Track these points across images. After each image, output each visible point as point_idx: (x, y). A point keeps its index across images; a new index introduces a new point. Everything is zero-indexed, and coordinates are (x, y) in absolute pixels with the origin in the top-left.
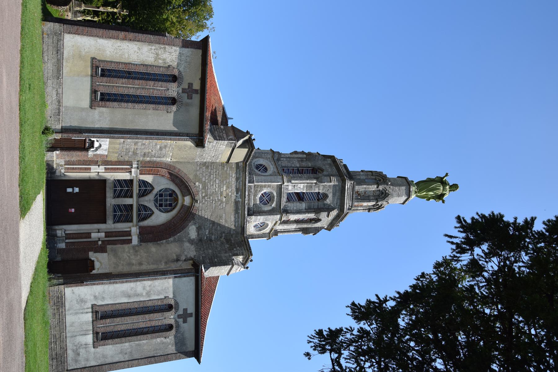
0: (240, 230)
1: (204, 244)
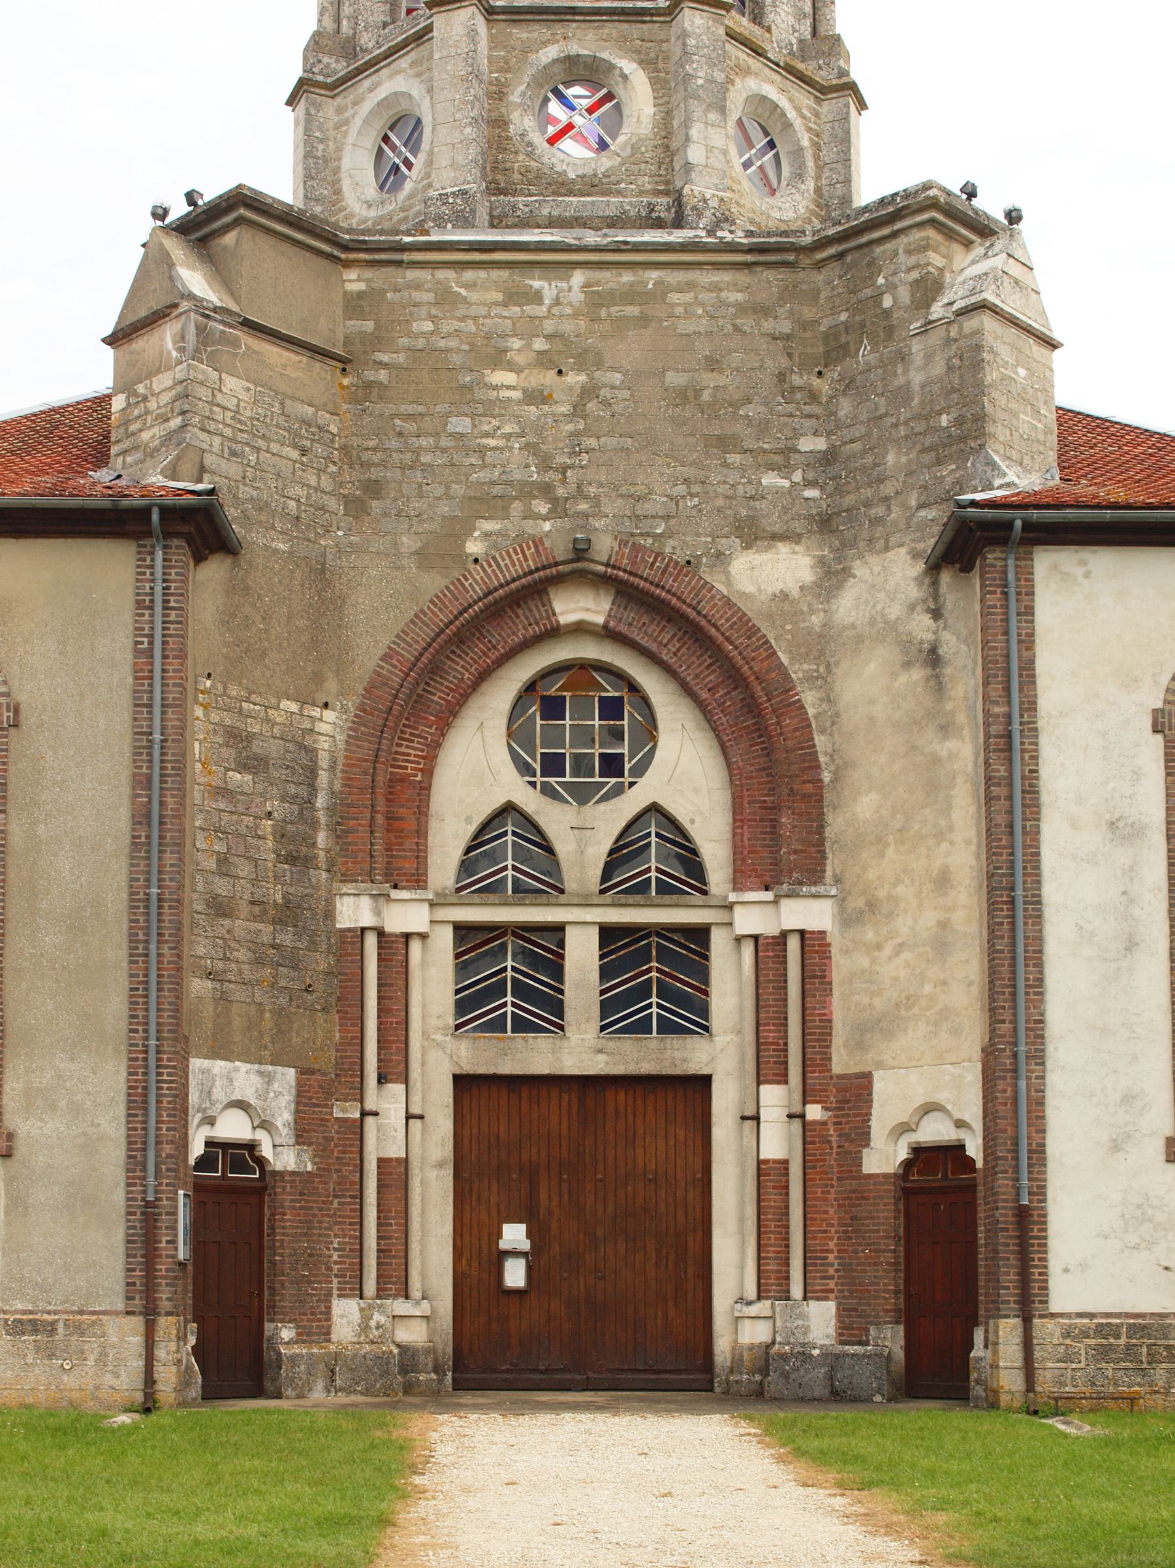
0: (770, 274)
1: (849, 500)
